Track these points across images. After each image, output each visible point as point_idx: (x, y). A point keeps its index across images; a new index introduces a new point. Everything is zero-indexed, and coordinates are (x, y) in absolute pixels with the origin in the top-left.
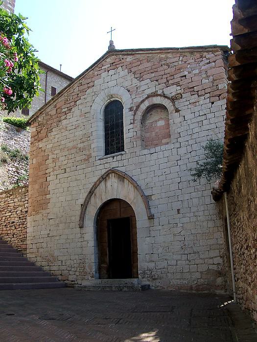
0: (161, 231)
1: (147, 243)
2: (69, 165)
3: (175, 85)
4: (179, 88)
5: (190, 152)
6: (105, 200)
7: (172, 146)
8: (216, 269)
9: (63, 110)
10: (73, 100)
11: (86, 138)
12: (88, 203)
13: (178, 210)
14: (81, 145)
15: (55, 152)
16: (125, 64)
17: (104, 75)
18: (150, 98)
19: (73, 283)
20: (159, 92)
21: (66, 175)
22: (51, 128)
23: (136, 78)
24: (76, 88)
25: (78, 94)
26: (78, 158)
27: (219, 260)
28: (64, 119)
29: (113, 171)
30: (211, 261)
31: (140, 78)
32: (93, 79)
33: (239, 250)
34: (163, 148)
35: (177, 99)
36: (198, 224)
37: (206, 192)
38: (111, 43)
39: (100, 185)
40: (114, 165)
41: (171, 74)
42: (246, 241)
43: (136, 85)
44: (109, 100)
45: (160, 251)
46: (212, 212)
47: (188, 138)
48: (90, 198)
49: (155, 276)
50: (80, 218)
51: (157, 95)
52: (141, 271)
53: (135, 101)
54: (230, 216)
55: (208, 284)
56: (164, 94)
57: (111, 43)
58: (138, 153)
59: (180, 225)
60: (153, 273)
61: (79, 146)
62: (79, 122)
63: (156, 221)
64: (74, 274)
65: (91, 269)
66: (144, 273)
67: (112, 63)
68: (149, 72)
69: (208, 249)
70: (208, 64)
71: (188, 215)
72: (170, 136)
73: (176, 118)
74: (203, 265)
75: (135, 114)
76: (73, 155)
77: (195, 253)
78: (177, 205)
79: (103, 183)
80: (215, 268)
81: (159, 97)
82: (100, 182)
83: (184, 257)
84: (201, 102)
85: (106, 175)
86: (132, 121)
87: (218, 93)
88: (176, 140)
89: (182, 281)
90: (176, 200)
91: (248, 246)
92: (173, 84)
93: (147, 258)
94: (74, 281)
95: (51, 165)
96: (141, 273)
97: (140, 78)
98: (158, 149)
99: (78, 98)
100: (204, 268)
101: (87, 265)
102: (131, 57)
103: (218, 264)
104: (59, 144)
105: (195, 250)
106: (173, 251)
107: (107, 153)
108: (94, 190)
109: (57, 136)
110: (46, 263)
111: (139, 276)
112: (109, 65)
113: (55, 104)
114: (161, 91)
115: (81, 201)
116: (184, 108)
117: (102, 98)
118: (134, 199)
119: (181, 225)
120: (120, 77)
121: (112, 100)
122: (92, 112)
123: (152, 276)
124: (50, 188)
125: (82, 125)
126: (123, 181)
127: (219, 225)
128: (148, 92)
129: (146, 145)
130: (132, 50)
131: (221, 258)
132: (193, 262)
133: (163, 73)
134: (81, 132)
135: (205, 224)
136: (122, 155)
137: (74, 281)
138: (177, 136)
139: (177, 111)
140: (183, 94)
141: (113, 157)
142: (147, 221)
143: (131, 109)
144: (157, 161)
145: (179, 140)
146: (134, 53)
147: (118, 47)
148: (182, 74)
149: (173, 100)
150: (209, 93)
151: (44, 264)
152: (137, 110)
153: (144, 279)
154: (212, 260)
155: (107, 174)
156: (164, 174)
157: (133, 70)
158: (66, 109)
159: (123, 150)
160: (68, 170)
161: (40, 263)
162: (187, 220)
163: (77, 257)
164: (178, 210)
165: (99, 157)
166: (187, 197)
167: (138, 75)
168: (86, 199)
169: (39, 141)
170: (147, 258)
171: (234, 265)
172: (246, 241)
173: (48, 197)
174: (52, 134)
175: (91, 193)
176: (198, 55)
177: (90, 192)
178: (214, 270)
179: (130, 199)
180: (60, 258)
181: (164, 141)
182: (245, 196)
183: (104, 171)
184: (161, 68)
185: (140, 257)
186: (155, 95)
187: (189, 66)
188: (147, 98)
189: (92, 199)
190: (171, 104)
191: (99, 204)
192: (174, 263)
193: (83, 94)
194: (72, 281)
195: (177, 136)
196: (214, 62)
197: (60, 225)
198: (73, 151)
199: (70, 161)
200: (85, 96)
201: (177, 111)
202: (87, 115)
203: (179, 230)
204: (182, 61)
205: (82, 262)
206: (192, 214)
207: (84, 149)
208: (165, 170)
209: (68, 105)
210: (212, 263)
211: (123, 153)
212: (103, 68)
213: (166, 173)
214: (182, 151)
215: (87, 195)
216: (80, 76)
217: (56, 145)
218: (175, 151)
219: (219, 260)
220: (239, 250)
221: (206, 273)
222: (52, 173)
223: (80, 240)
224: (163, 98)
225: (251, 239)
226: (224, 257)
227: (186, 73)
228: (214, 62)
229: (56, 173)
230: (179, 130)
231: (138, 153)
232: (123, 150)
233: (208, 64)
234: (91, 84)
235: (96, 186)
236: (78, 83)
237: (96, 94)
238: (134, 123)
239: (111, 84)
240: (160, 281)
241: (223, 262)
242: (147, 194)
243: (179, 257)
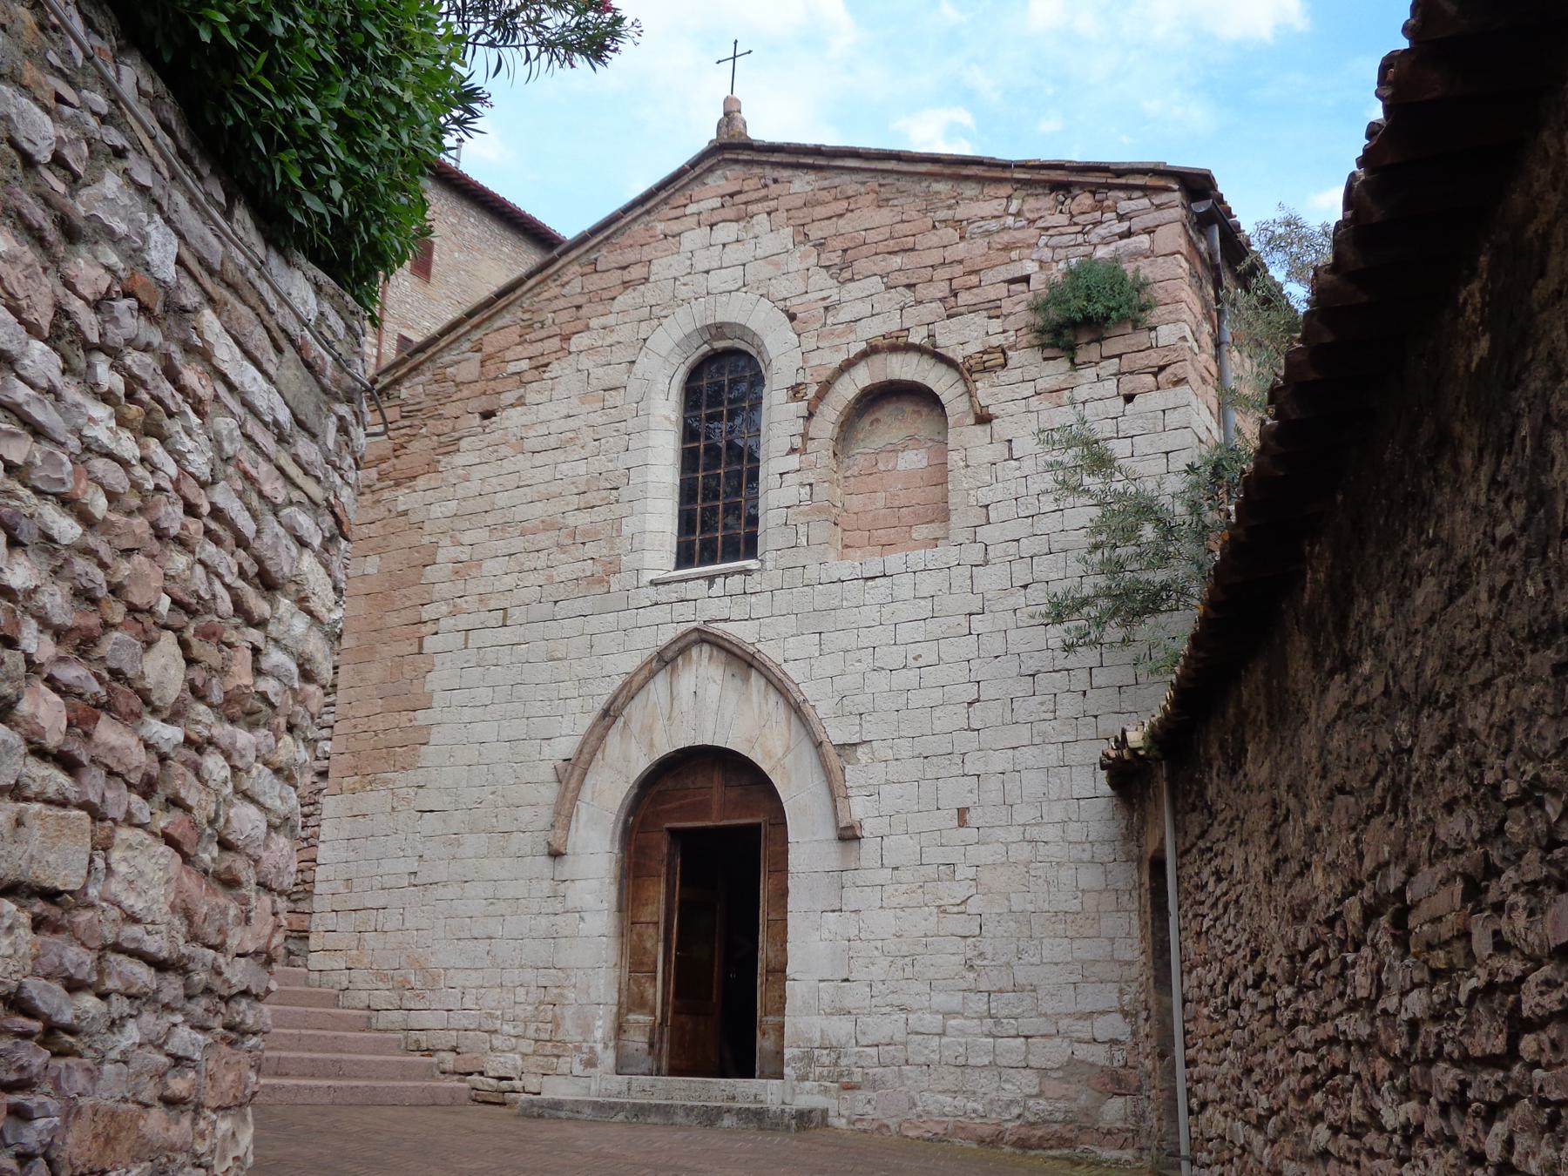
0: (890, 890)
1: (826, 935)
2: (525, 595)
3: (985, 313)
4: (995, 326)
5: (1025, 587)
6: (664, 748)
7: (946, 554)
8: (1101, 1063)
9: (512, 368)
10: (557, 330)
11: (604, 493)
12: (593, 754)
13: (962, 813)
14: (583, 519)
16: (785, 202)
17: (694, 238)
18: (877, 360)
19: (504, 1084)
20: (916, 338)
21: (505, 635)
22: (457, 435)
23: (827, 267)
24: (573, 279)
26: (565, 571)
27: (1115, 1026)
28: (512, 405)
29: (703, 638)
30: (1082, 1029)
31: (843, 271)
32: (647, 252)
33: (1218, 987)
34: (917, 557)
35: (985, 370)
36: (1038, 873)
37: (1078, 748)
38: (730, 114)
39: (651, 686)
40: (713, 609)
41: (968, 266)
42: (1255, 953)
43: (824, 294)
44: (706, 348)
45: (877, 971)
46: (1097, 830)
48: (602, 738)
49: (850, 1074)
50: (557, 813)
51: (910, 348)
52: (796, 1051)
53: (815, 360)
54: (1182, 854)
55: (1065, 1122)
57: (730, 114)
58: (812, 573)
59: (963, 872)
60: (844, 1062)
61: (571, 520)
62: (572, 423)
63: (869, 847)
64: (513, 1050)
65: (587, 1029)
66: (808, 1058)
67: (732, 195)
68: (881, 247)
69: (1076, 978)
70: (1122, 236)
71: (1000, 834)
72: (944, 515)
73: (968, 441)
74: (1049, 1043)
75: (811, 414)
77: (1017, 988)
78: (956, 792)
79: (661, 681)
80: (1098, 1055)
81: (913, 358)
82: (652, 675)
83: (978, 1004)
84: (1082, 393)
85: (675, 648)
86: (798, 442)
87: (1155, 359)
88: (968, 533)
89: (960, 1101)
90: (956, 770)
91: (1260, 978)
92: (973, 309)
93: (826, 998)
94: (511, 1079)
96: (794, 1059)
97: (843, 271)
98: (894, 561)
99: (580, 325)
100: (1053, 1052)
101: (569, 1013)
102: (811, 176)
103: (1114, 1042)
105: (1021, 979)
106: (930, 974)
107: (685, 557)
108: (624, 705)
109: (477, 473)
110: (394, 995)
111: (787, 1070)
112: (717, 202)
113: (476, 335)
114: (924, 331)
115: (566, 746)
117: (678, 335)
118: (785, 755)
119: (971, 873)
120: (760, 253)
121: (720, 345)
122: (634, 386)
123: (841, 1075)
124: (434, 682)
125: (587, 435)
126: (746, 680)
127: (1120, 885)
128: (873, 329)
129: (847, 541)
130: (817, 151)
131: (1125, 1016)
132: (1010, 1026)
133: (935, 257)
134: (582, 468)
135: (1066, 874)
136: (747, 572)
137: (511, 1079)
138: (977, 516)
139: (984, 419)
140: (1010, 353)
141: (711, 579)
142: (834, 848)
143: (796, 391)
144: (886, 610)
145: (985, 533)
146: (822, 162)
147: (762, 129)
148: (1016, 271)
149: (965, 371)
150: (1119, 356)
151: (382, 998)
152: (820, 397)
153: (808, 1084)
154: (1088, 1023)
155: (680, 644)
157: (816, 232)
158: (525, 365)
159: (751, 552)
160: (516, 614)
161: (364, 994)
162: (984, 854)
163: (529, 975)
164: (962, 813)
165: (653, 575)
166: (1000, 761)
167: (835, 258)
168: (584, 743)
169: (398, 484)
170: (826, 998)
171: (1186, 1047)
172: (1255, 953)
173: (421, 717)
174: (458, 460)
175: (609, 715)
176: (1085, 200)
177: (606, 713)
178: (1092, 1065)
179: (768, 754)
180: (458, 979)
182: (1261, 789)
183: (668, 634)
184: (933, 239)
185: (796, 991)
186: (898, 346)
187: (1044, 240)
188: (864, 355)
189: (613, 738)
190: (960, 388)
191: (641, 764)
192: (932, 1022)
193: (600, 308)
194: (501, 1079)
195: (977, 516)
196: (1150, 231)
197: (470, 840)
198: (544, 540)
199: (531, 578)
200: (610, 320)
201: (984, 419)
202: (614, 398)
204: (1018, 214)
205: (547, 999)
206: (1016, 834)
207: (591, 536)
209: (533, 350)
210: (1088, 1037)
211: (751, 564)
212: (689, 210)
213: (921, 662)
214: (991, 579)
215: (594, 726)
216: (595, 231)
217: (470, 506)
218: (960, 576)
219: (1115, 1026)
220: (1218, 987)
221: (1061, 1074)
222: (445, 623)
223: (548, 907)
225: (1279, 949)
226: (1136, 1015)
227: (1030, 267)
228: (1150, 231)
229: (463, 621)
230: (985, 496)
232: (751, 552)
233: (1122, 236)
234: (636, 273)
235: (631, 690)
236: (584, 260)
237: (654, 316)
239: (716, 281)
241: (1134, 1034)
243: (955, 1001)
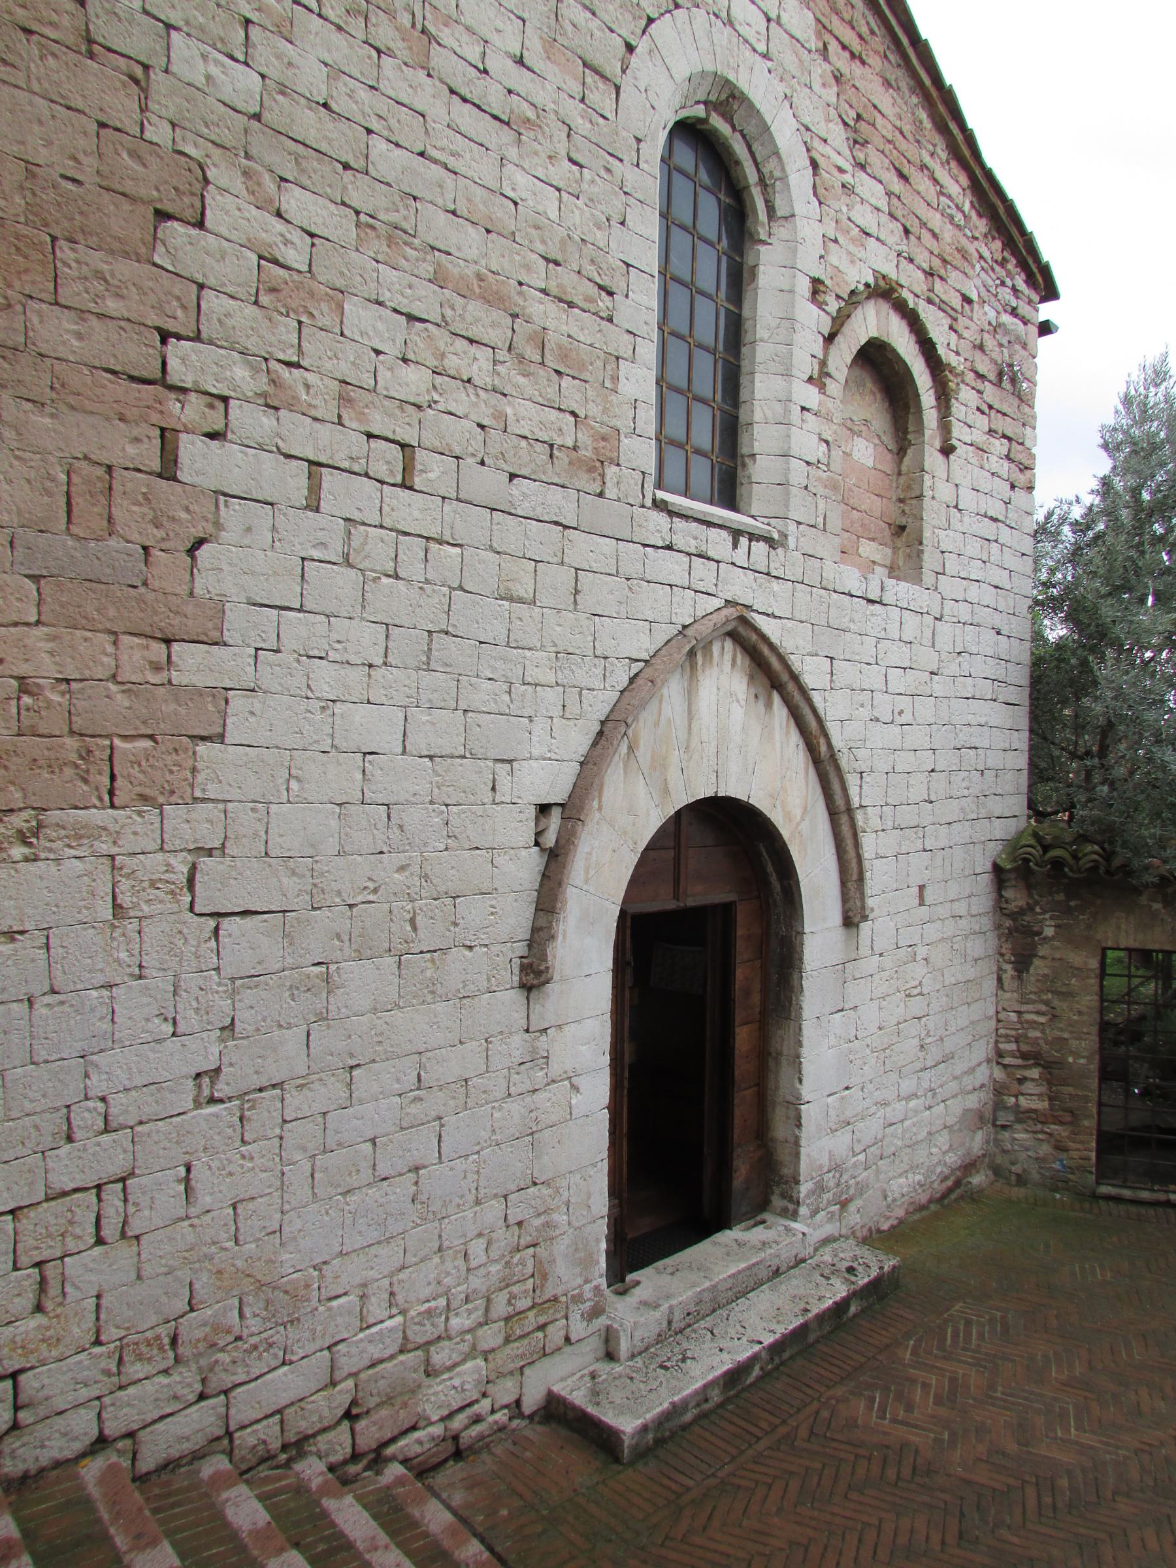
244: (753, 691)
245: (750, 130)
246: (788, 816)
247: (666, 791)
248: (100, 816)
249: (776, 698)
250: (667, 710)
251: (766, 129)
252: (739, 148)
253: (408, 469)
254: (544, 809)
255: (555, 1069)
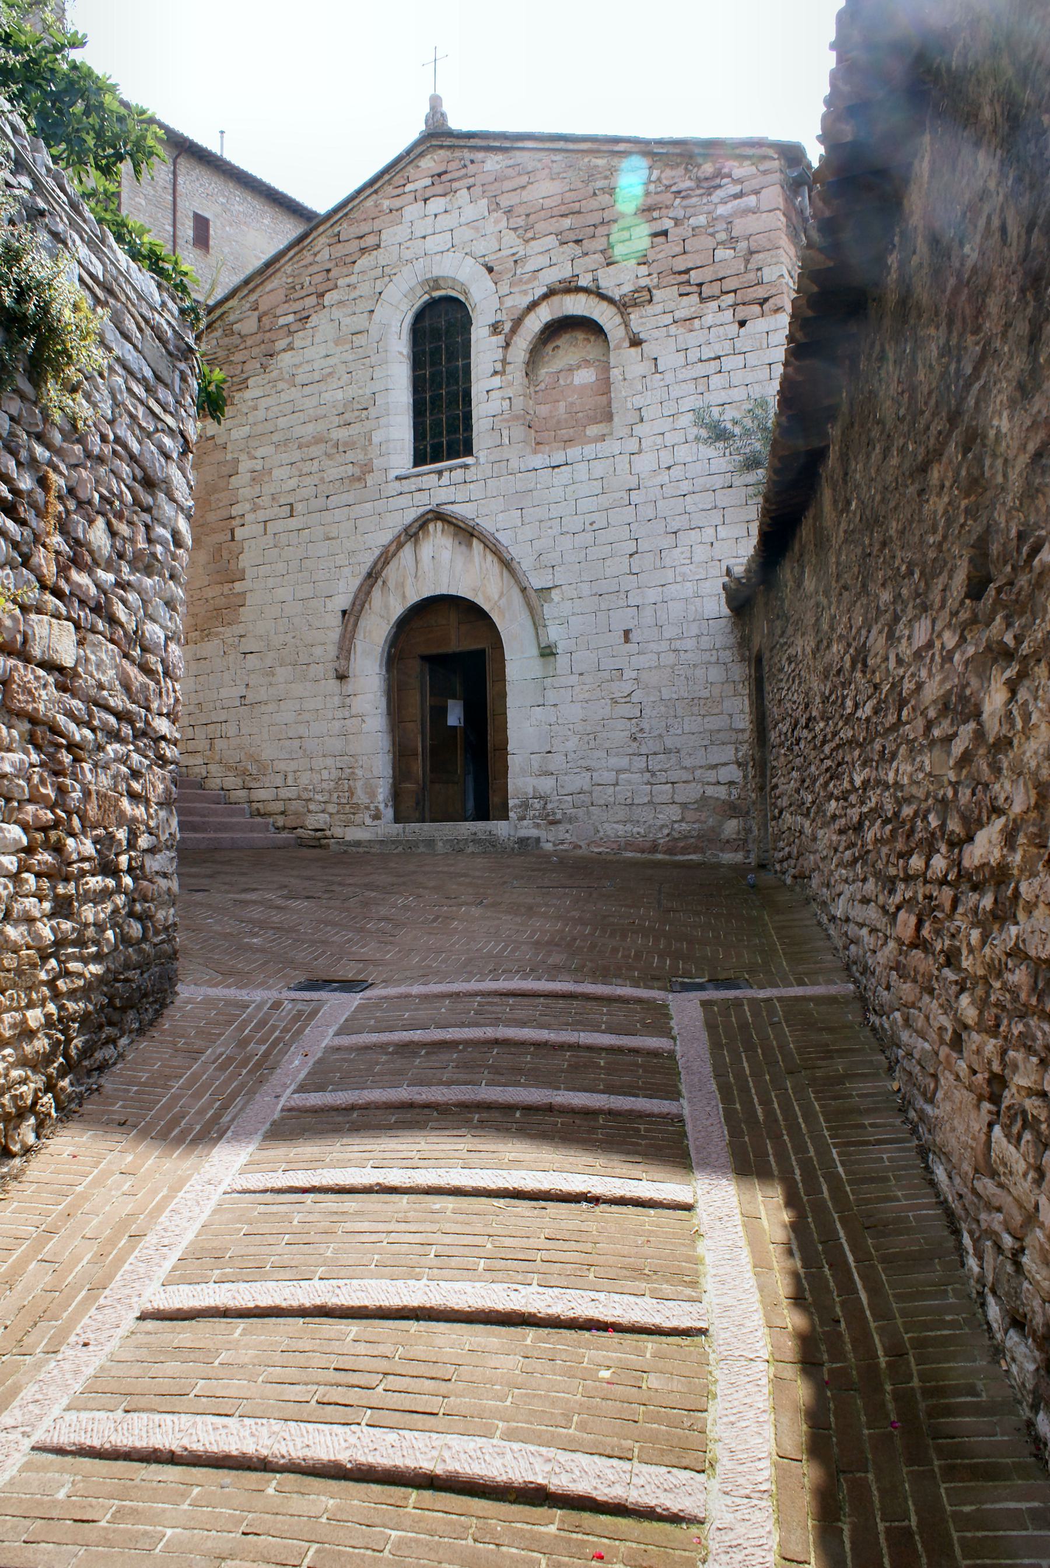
0: (577, 689)
9: (282, 321)
11: (357, 413)
12: (363, 606)
13: (627, 633)
15: (259, 453)
17: (412, 211)
18: (555, 299)
19: (319, 834)
21: (294, 523)
22: (244, 376)
23: (515, 229)
25: (328, 271)
30: (711, 776)
32: (377, 225)
34: (589, 450)
35: (636, 305)
39: (401, 554)
44: (426, 297)
47: (665, 425)
48: (368, 593)
49: (554, 814)
50: (341, 648)
52: (517, 801)
53: (509, 302)
55: (699, 837)
56: (598, 288)
58: (514, 464)
59: (629, 674)
60: (549, 806)
63: (562, 661)
64: (323, 811)
65: (372, 795)
67: (439, 175)
68: (556, 212)
76: (316, 462)
77: (666, 751)
80: (721, 792)
81: (582, 297)
82: (400, 546)
84: (709, 320)
88: (627, 430)
89: (629, 827)
95: (246, 492)
96: (515, 806)
98: (573, 453)
99: (330, 284)
102: (499, 157)
103: (731, 783)
104: (269, 426)
107: (420, 458)
109: (263, 403)
111: (511, 814)
112: (428, 181)
114: (589, 277)
116: (656, 333)
119: (634, 674)
120: (463, 220)
124: (245, 561)
125: (342, 369)
128: (552, 277)
139: (636, 342)
143: (495, 328)
156: (588, 527)
157: (505, 201)
164: (627, 633)
167: (520, 222)
173: (238, 586)
174: (248, 394)
177: (369, 575)
180: (281, 766)
181: (593, 430)
183: (411, 515)
189: (376, 593)
190: (618, 319)
191: (397, 609)
192: (609, 777)
193: (345, 270)
198: (315, 451)
199: (308, 481)
200: (353, 279)
201: (636, 342)
202: (360, 340)
203: (627, 687)
208: (594, 517)
211: (469, 460)
213: (595, 526)
217: (259, 428)
222: (250, 517)
223: (339, 714)
224: (593, 300)
227: (668, 224)
230: (638, 401)
231: (514, 464)
236: (330, 232)
238: (503, 373)
240: (569, 827)
242: (537, 581)
243: (624, 762)
244: (457, 542)
245: (450, 284)
246: (488, 599)
247: (404, 597)
248: (220, 629)
249: (475, 541)
250: (403, 561)
251: (454, 279)
252: (453, 294)
253: (292, 510)
254: (344, 612)
255: (354, 712)
